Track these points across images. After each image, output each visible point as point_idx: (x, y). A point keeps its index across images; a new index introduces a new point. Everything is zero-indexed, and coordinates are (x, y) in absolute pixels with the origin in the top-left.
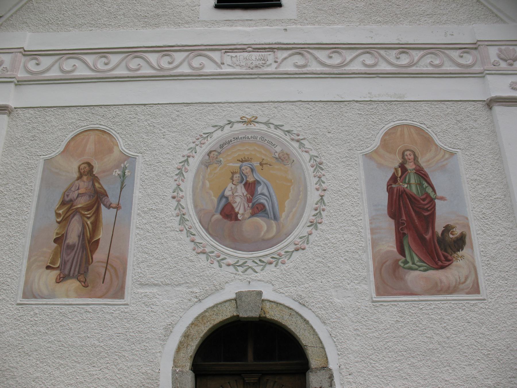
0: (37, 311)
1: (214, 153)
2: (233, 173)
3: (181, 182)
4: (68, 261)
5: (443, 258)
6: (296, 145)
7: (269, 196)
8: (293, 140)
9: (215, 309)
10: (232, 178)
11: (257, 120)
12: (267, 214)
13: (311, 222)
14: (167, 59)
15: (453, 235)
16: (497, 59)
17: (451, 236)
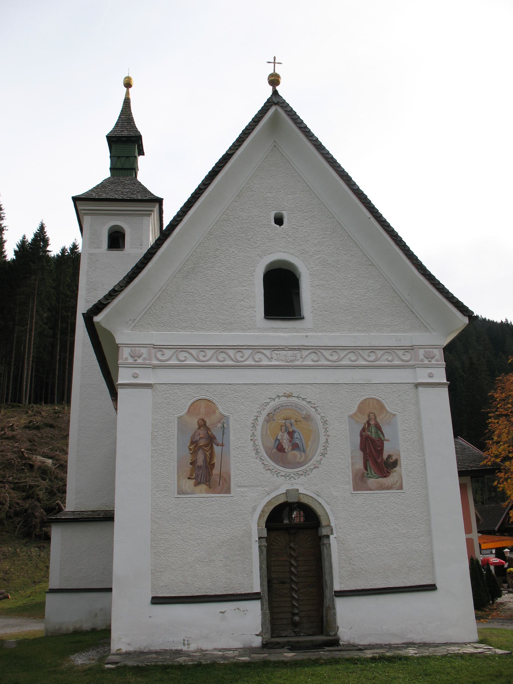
0: (186, 501)
1: (271, 414)
2: (282, 426)
3: (254, 431)
4: (199, 474)
5: (386, 472)
6: (313, 410)
7: (300, 439)
8: (312, 407)
9: (276, 498)
10: (281, 429)
11: (292, 395)
12: (300, 449)
13: (322, 453)
14: (240, 354)
15: (392, 460)
16: (423, 358)
17: (391, 460)
